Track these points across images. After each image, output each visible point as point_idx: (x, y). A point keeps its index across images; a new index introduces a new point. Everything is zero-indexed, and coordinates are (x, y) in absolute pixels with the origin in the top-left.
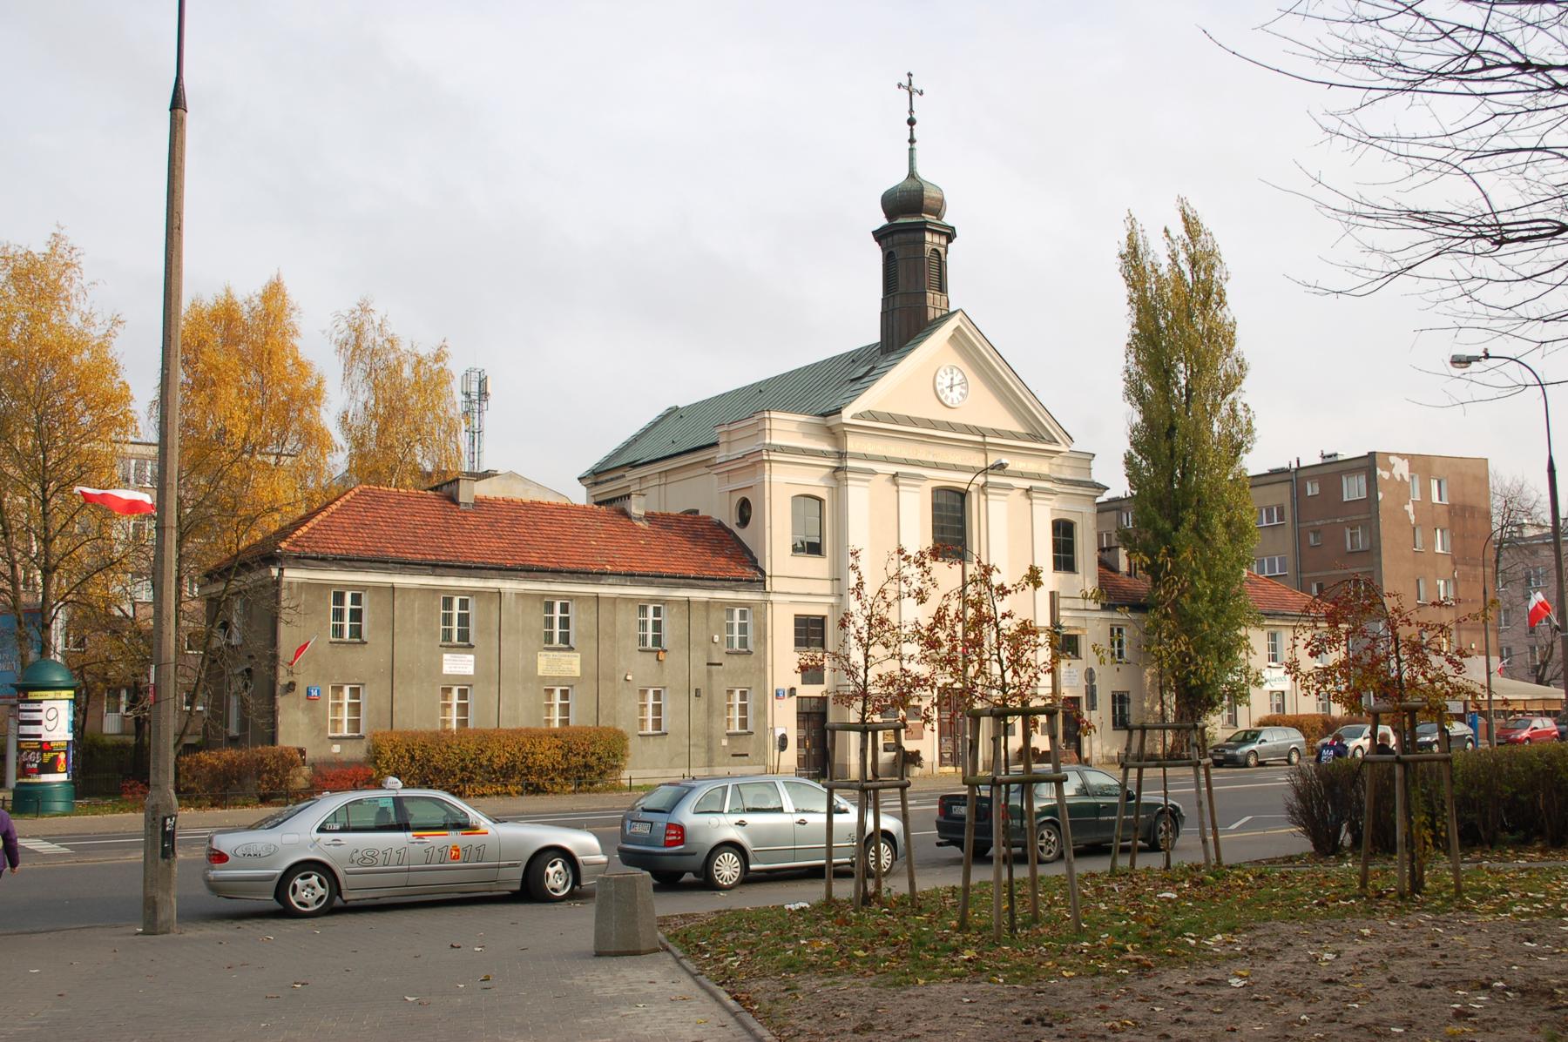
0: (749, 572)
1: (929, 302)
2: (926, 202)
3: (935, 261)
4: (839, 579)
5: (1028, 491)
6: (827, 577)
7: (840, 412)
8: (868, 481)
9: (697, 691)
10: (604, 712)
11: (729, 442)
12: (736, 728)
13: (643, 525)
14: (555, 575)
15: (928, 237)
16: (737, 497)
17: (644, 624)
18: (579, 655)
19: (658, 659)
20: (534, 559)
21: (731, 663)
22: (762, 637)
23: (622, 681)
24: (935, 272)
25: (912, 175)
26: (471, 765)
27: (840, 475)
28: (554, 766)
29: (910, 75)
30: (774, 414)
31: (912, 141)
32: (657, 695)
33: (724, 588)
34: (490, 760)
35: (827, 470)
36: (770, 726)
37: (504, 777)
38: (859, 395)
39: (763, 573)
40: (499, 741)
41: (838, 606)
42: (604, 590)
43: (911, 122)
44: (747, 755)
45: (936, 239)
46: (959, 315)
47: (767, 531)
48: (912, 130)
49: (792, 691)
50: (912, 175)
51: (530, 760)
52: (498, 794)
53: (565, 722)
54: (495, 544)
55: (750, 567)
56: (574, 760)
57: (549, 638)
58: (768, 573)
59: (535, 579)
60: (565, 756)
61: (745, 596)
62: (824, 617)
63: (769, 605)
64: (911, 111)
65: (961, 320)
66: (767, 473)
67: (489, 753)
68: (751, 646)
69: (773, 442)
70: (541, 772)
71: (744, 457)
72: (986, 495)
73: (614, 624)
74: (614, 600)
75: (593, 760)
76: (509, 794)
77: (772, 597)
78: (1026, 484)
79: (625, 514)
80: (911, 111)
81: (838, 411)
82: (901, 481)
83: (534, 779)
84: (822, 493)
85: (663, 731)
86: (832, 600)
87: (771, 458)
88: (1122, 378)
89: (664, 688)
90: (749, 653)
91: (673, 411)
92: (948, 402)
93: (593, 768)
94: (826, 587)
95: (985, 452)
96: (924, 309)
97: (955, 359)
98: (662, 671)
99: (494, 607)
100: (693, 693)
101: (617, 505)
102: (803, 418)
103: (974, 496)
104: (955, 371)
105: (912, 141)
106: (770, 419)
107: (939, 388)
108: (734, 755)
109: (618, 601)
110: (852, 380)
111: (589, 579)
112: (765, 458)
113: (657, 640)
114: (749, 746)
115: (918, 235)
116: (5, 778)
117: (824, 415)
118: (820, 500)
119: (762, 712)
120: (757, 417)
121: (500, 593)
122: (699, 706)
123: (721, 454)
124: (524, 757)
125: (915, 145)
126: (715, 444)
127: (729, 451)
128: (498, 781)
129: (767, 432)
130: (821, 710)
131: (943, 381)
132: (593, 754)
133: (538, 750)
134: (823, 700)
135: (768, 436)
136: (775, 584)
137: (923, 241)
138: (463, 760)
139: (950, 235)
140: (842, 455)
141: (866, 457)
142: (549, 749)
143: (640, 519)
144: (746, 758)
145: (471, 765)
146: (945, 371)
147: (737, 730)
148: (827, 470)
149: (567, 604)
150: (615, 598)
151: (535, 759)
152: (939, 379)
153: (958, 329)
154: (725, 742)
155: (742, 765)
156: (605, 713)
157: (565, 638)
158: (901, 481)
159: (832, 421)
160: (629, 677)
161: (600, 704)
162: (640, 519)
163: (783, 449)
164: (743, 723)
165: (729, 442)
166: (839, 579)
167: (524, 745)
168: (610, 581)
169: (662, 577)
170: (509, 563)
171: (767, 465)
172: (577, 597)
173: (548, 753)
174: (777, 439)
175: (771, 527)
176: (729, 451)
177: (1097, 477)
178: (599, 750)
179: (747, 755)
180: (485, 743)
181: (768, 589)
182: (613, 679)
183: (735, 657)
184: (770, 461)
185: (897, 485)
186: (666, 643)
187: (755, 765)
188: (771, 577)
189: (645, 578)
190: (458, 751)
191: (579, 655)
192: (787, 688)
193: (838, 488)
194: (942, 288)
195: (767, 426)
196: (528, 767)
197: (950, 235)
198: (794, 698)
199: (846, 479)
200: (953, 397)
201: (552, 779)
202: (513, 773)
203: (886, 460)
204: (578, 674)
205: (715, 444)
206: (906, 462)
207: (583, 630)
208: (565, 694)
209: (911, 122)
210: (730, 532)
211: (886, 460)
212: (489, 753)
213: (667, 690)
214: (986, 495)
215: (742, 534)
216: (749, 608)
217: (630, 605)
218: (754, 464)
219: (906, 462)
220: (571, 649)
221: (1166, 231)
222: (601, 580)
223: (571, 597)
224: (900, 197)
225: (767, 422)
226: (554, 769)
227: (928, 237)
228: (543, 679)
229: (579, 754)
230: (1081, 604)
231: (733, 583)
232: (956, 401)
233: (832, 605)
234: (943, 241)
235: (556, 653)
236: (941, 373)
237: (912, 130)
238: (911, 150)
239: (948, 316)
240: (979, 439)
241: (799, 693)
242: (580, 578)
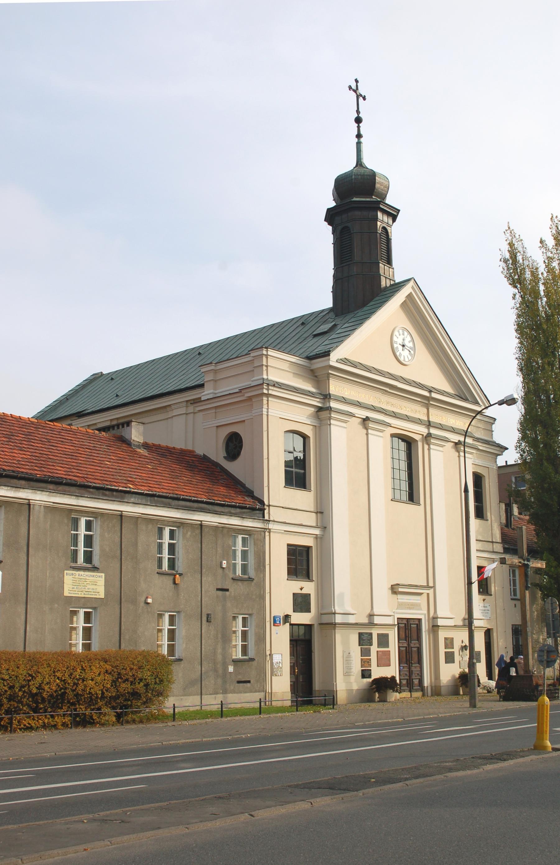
0: (249, 502)
1: (381, 272)
2: (377, 186)
3: (384, 237)
4: (322, 513)
5: (366, 420)
6: (312, 510)
7: (329, 355)
8: (346, 422)
9: (208, 615)
10: (126, 636)
11: (215, 381)
12: (239, 655)
13: (142, 451)
14: (82, 491)
15: (380, 215)
16: (224, 433)
17: (160, 546)
18: (103, 575)
19: (174, 583)
20: (60, 472)
21: (236, 589)
22: (261, 565)
23: (142, 604)
24: (384, 247)
25: (359, 163)
26: (20, 694)
27: (324, 414)
28: (103, 693)
29: (357, 81)
30: (271, 352)
31: (359, 136)
32: (172, 620)
33: (231, 515)
34: (40, 688)
35: (312, 410)
36: (268, 653)
37: (51, 708)
38: (342, 341)
39: (262, 502)
40: (49, 665)
41: (321, 538)
42: (128, 509)
43: (358, 120)
44: (249, 682)
45: (385, 218)
46: (412, 283)
47: (265, 462)
48: (359, 127)
49: (287, 618)
50: (359, 163)
51: (80, 687)
52: (44, 726)
53: (87, 647)
54: (19, 455)
55: (248, 496)
56: (125, 687)
57: (75, 559)
58: (266, 503)
59: (64, 493)
60: (114, 682)
61: (249, 523)
62: (308, 549)
63: (267, 534)
64: (358, 112)
65: (413, 288)
66: (265, 406)
67: (39, 679)
68: (252, 572)
69: (271, 378)
70: (91, 701)
71: (241, 390)
72: (429, 445)
73: (136, 544)
74: (136, 520)
75: (140, 687)
76: (55, 726)
77: (271, 526)
78: (456, 438)
79: (125, 441)
80: (358, 112)
81: (327, 354)
82: (371, 425)
83: (82, 709)
84: (308, 431)
85: (177, 657)
86: (317, 532)
87: (270, 392)
88: (515, 356)
89: (178, 612)
90: (250, 579)
91: (97, 378)
92: (402, 359)
93: (140, 696)
94: (311, 519)
95: (427, 406)
96: (377, 277)
97: (404, 321)
98: (178, 595)
99: (23, 519)
100: (204, 619)
101: (116, 432)
102: (293, 359)
103: (420, 444)
104: (406, 333)
105: (359, 136)
106: (267, 356)
107: (395, 346)
108: (239, 682)
109: (140, 520)
110: (315, 336)
111: (113, 496)
112: (265, 391)
113: (172, 563)
114: (251, 674)
115: (371, 214)
116: (474, 671)
117: (310, 358)
118: (305, 437)
119: (261, 639)
120: (252, 355)
121: (29, 505)
122: (209, 631)
123: (207, 393)
124: (75, 684)
125: (362, 140)
126: (202, 386)
127: (215, 389)
128: (46, 711)
129: (265, 368)
130: (307, 637)
131: (398, 340)
132: (141, 680)
133: (89, 675)
134: (309, 628)
135: (265, 372)
136: (273, 514)
137: (376, 219)
138: (12, 687)
139: (393, 214)
140: (327, 397)
141: (344, 401)
142: (99, 674)
143: (139, 447)
144: (248, 685)
145: (20, 694)
146: (399, 331)
147: (240, 656)
148: (312, 410)
149: (90, 521)
150: (137, 518)
151: (86, 686)
152: (395, 339)
153: (410, 296)
154: (231, 669)
155: (246, 692)
156: (127, 637)
157: (88, 557)
158: (371, 425)
159: (318, 363)
160: (150, 601)
161: (123, 628)
162: (139, 447)
163: (280, 386)
164: (245, 649)
165: (215, 381)
166: (322, 513)
167: (74, 669)
168: (132, 500)
169: (178, 499)
170: (39, 474)
171: (265, 399)
172: (102, 514)
173: (99, 679)
174: (273, 376)
175: (268, 458)
176: (215, 389)
177: (498, 438)
178: (146, 674)
179: (249, 682)
180: (35, 668)
181: (266, 517)
182: (134, 602)
183: (240, 583)
184: (268, 395)
185: (366, 428)
186: (180, 566)
187: (256, 692)
188: (269, 506)
189: (163, 499)
190: (7, 677)
191: (103, 575)
192: (282, 615)
193: (320, 427)
194: (389, 261)
195: (264, 363)
196: (77, 695)
197: (393, 214)
198: (288, 625)
199: (330, 418)
200: (404, 355)
201: (99, 709)
202: (62, 703)
203: (359, 405)
204: (102, 596)
205: (202, 386)
206: (373, 409)
207: (107, 549)
208: (88, 616)
209: (358, 120)
210: (217, 465)
211: (359, 405)
212: (39, 679)
213: (183, 615)
214: (429, 445)
215: (232, 467)
216: (250, 535)
217: (150, 526)
218: (250, 398)
219: (373, 409)
220: (95, 569)
221: (542, 242)
222: (123, 498)
223: (97, 514)
224: (355, 179)
225: (264, 359)
226: (103, 697)
227: (380, 215)
228: (69, 600)
229: (127, 680)
230: (489, 547)
231: (238, 510)
232: (407, 360)
233: (316, 537)
234: (390, 221)
235: (82, 573)
236: (396, 333)
237: (359, 127)
238: (359, 144)
239: (397, 287)
240: (426, 394)
241: (293, 621)
242: (106, 495)
